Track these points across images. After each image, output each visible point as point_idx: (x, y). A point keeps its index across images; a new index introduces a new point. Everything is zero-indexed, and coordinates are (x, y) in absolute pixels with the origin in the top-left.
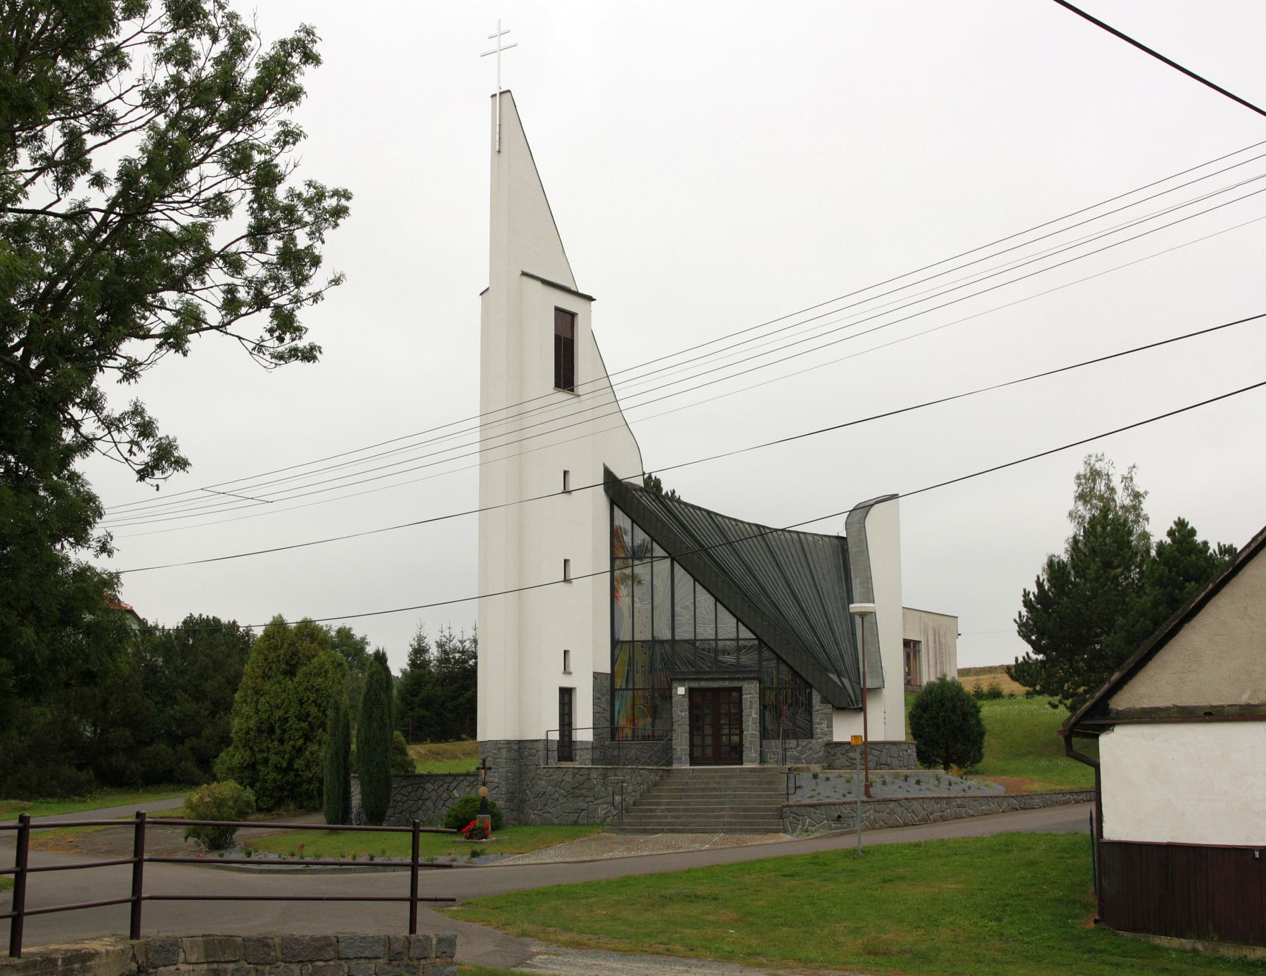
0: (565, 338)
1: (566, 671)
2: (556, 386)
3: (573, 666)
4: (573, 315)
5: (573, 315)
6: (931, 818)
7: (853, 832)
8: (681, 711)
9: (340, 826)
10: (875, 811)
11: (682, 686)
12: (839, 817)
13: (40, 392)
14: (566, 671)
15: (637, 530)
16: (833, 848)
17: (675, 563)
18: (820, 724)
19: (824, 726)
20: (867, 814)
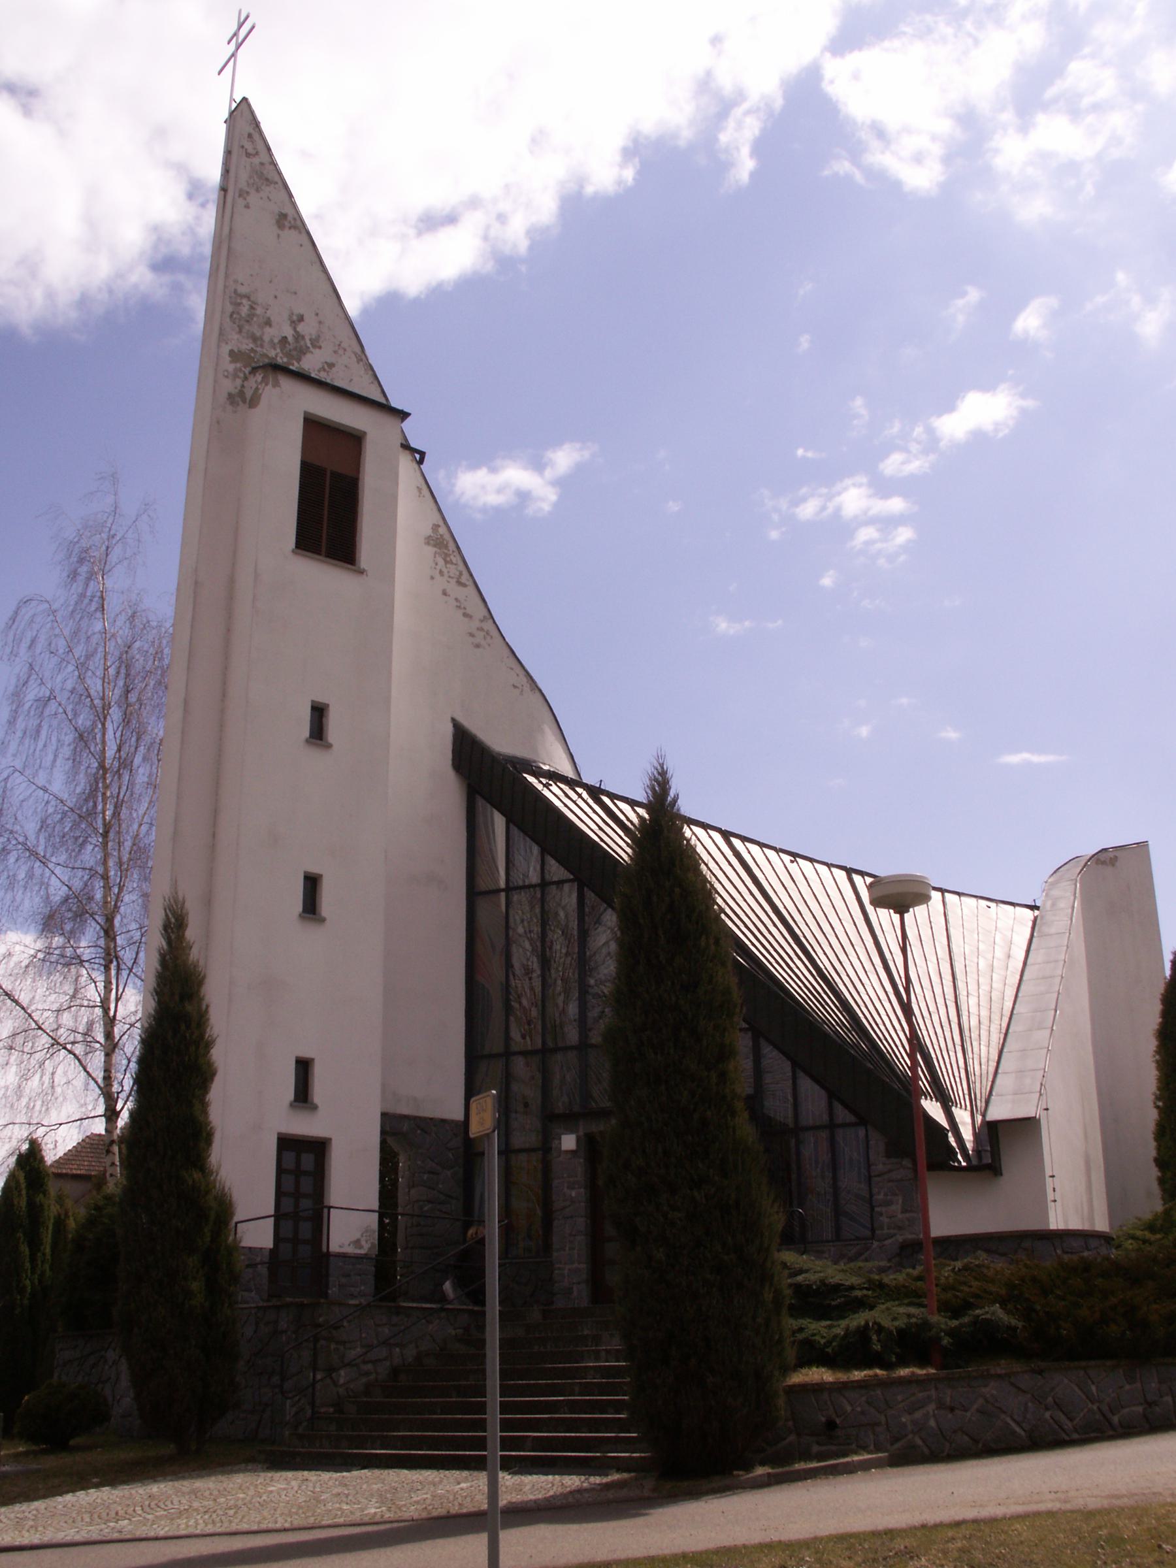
0: (333, 473)
1: (303, 1095)
2: (296, 547)
3: (319, 1090)
4: (354, 440)
5: (354, 440)
6: (1116, 1419)
7: (477, 1464)
8: (571, 1188)
9: (814, 1465)
10: (941, 1405)
11: (572, 1132)
12: (831, 1425)
13: (63, 934)
14: (303, 1095)
15: (807, 1085)
16: (827, 1534)
17: (763, 1042)
18: (888, 1203)
19: (896, 1208)
20: (918, 1415)
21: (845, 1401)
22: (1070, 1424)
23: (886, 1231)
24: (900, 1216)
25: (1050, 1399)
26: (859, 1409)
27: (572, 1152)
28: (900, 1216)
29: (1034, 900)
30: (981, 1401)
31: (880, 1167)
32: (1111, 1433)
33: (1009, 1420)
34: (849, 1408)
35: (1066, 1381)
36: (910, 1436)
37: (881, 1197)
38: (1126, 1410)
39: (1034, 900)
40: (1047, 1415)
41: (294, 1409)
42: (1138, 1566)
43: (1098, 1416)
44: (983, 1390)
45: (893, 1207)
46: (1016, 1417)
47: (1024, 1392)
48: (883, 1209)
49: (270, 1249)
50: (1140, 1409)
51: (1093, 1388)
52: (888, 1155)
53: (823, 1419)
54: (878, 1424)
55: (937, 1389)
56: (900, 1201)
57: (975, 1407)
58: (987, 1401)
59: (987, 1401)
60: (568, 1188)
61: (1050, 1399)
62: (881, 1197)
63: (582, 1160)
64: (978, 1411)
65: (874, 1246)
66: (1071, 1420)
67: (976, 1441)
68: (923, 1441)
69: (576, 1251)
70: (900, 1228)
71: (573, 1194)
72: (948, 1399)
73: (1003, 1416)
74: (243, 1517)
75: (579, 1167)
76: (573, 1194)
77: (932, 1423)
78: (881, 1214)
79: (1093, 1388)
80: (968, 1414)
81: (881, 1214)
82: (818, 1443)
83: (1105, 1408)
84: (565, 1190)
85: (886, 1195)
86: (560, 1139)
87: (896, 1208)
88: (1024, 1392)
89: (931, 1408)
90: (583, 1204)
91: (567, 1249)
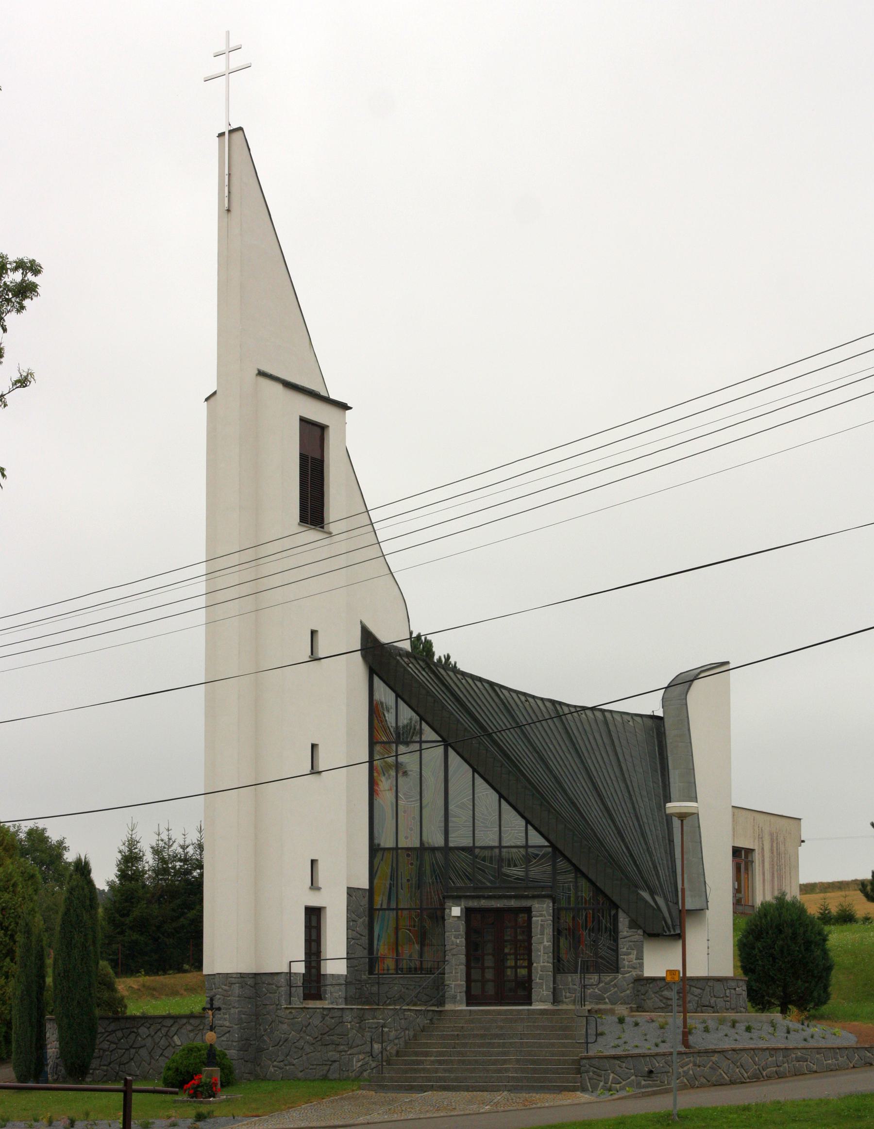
1: (314, 886)
6: (764, 1074)
8: (456, 937)
10: (695, 1065)
11: (458, 905)
12: (651, 1072)
14: (314, 886)
18: (628, 954)
19: (633, 956)
20: (685, 1068)
21: (655, 1061)
22: (746, 1074)
23: (626, 969)
24: (635, 961)
25: (739, 1064)
26: (661, 1065)
27: (458, 917)
28: (635, 961)
29: (653, 711)
30: (711, 1063)
31: (625, 933)
32: (762, 1079)
33: (722, 1072)
34: (657, 1065)
35: (746, 1055)
36: (682, 1078)
37: (625, 950)
38: (769, 1069)
39: (653, 711)
40: (737, 1070)
41: (360, 1064)
42: (195, 1128)
43: (758, 1071)
44: (713, 1058)
45: (631, 956)
46: (725, 1071)
47: (728, 1059)
48: (625, 957)
49: (303, 974)
50: (774, 1069)
51: (757, 1059)
52: (630, 928)
53: (647, 1069)
54: (669, 1072)
55: (693, 1057)
56: (635, 953)
57: (709, 1066)
58: (713, 1063)
59: (713, 1063)
60: (454, 937)
61: (739, 1064)
62: (625, 950)
63: (463, 922)
64: (710, 1068)
65: (620, 977)
66: (747, 1073)
67: (709, 1081)
68: (688, 1081)
69: (459, 975)
70: (635, 968)
71: (458, 942)
72: (698, 1062)
73: (720, 1070)
74: (176, 1107)
75: (462, 926)
76: (458, 942)
77: (691, 1072)
78: (624, 960)
79: (757, 1059)
80: (706, 1069)
81: (624, 960)
82: (645, 1080)
83: (761, 1069)
84: (453, 938)
85: (627, 949)
86: (451, 909)
87: (633, 956)
88: (728, 1059)
89: (691, 1065)
90: (464, 948)
91: (454, 972)
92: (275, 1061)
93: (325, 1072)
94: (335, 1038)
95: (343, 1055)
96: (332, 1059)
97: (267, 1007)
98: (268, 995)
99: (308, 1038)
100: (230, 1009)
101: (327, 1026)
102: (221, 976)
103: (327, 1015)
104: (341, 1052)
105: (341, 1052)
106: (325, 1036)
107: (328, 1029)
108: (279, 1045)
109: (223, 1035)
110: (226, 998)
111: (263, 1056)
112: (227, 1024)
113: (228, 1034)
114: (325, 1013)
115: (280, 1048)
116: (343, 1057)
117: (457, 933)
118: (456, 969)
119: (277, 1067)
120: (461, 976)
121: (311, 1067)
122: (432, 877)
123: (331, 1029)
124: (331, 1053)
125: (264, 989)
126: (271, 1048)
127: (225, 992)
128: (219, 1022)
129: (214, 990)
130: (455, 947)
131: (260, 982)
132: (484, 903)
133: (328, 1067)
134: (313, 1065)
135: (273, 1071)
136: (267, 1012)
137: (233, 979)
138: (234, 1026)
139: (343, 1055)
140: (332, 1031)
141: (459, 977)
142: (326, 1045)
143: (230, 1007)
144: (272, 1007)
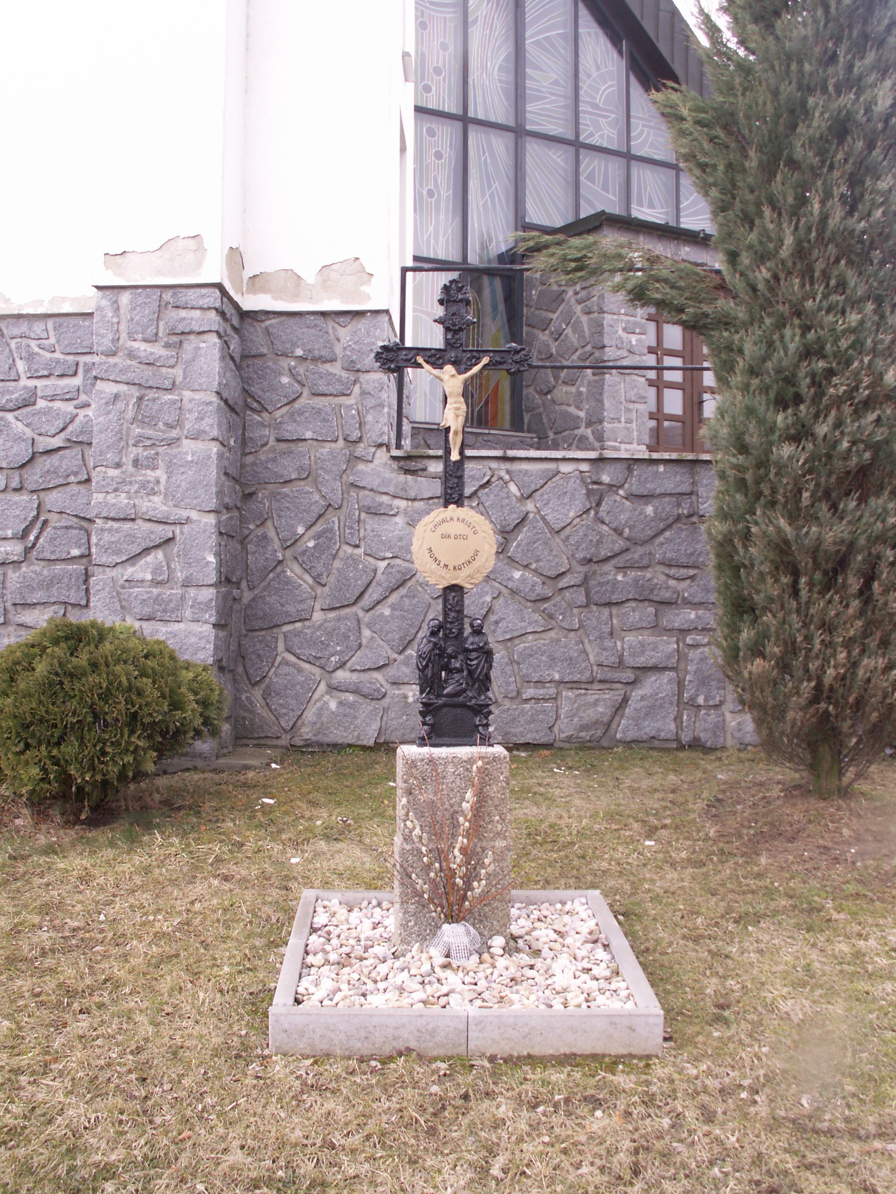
60: (624, 329)
69: (634, 425)
84: (620, 332)
92: (342, 665)
93: (602, 710)
94: (656, 575)
95: (696, 646)
96: (641, 661)
97: (301, 447)
98: (302, 401)
99: (517, 575)
100: (173, 442)
101: (618, 532)
102: (125, 298)
103: (613, 487)
104: (688, 631)
105: (688, 631)
106: (608, 567)
107: (620, 544)
108: (367, 601)
109: (133, 559)
110: (151, 394)
111: (281, 646)
112: (156, 505)
113: (160, 554)
114: (606, 479)
115: (366, 618)
116: (694, 654)
117: (631, 319)
118: (628, 410)
119: (356, 692)
120: (639, 431)
121: (529, 692)
122: (483, 195)
123: (634, 542)
124: (630, 638)
125: (285, 380)
126: (318, 616)
127: (148, 372)
128: (111, 498)
129: (24, 382)
130: (625, 354)
131: (264, 350)
132: (687, 253)
133: (620, 690)
134: (540, 683)
135: (333, 705)
136: (301, 469)
137: (197, 314)
138: (194, 515)
139: (696, 646)
140: (640, 550)
141: (635, 433)
142: (609, 604)
143: (174, 433)
144: (327, 448)
